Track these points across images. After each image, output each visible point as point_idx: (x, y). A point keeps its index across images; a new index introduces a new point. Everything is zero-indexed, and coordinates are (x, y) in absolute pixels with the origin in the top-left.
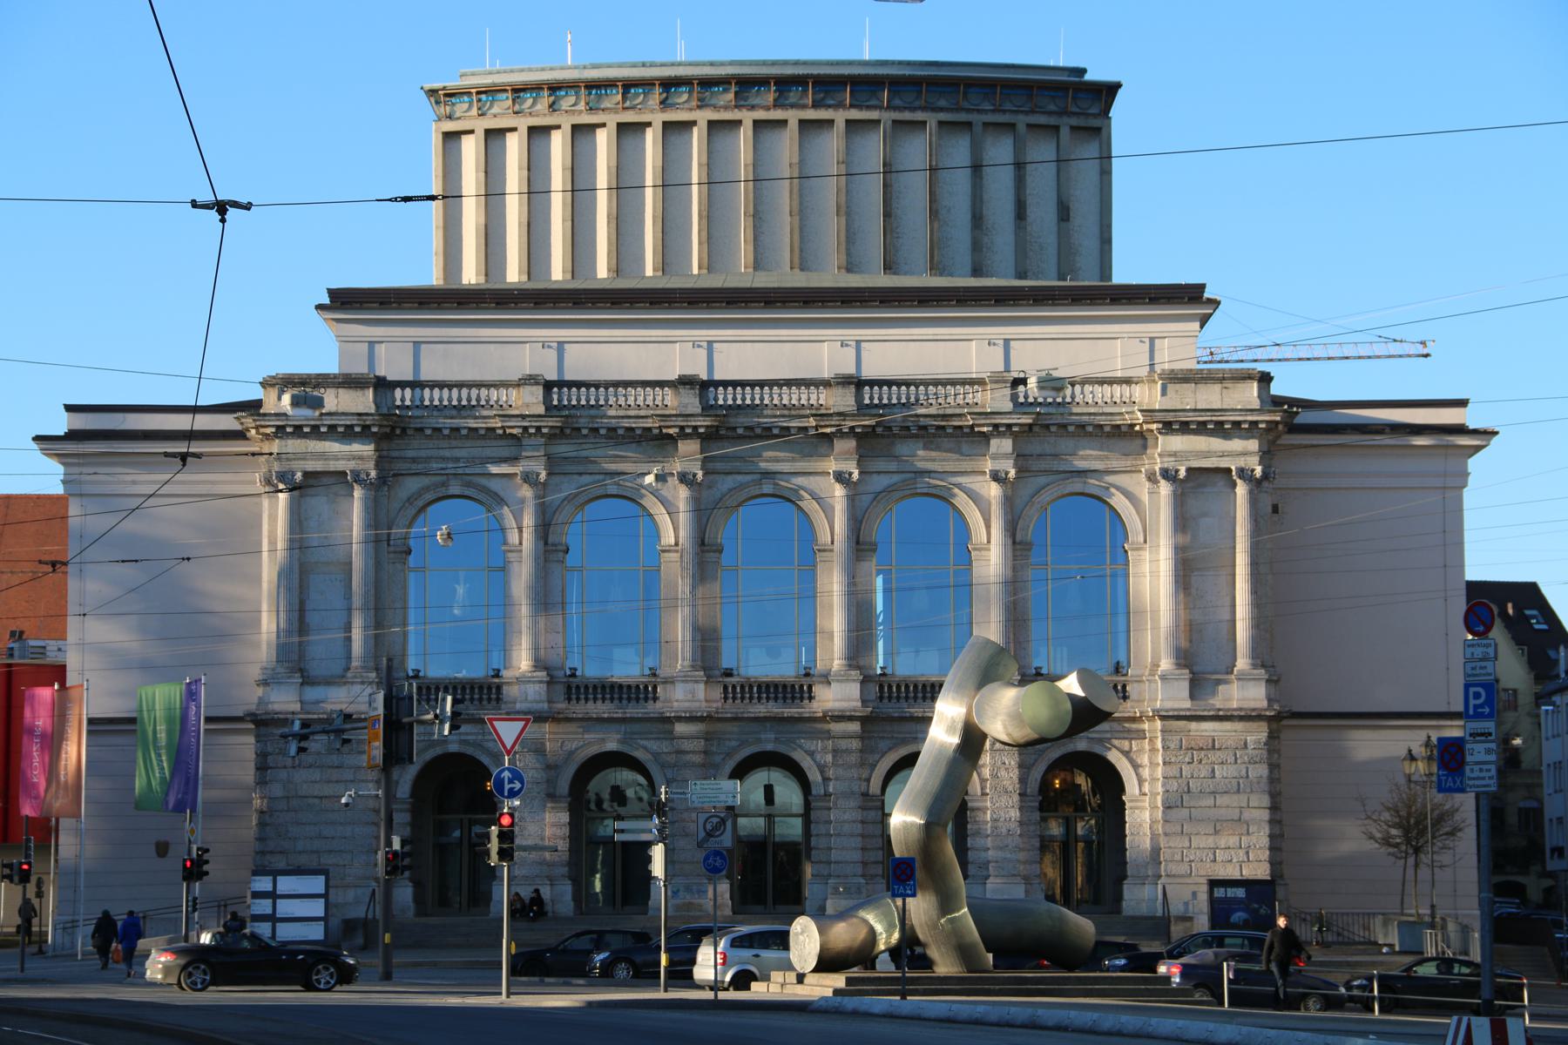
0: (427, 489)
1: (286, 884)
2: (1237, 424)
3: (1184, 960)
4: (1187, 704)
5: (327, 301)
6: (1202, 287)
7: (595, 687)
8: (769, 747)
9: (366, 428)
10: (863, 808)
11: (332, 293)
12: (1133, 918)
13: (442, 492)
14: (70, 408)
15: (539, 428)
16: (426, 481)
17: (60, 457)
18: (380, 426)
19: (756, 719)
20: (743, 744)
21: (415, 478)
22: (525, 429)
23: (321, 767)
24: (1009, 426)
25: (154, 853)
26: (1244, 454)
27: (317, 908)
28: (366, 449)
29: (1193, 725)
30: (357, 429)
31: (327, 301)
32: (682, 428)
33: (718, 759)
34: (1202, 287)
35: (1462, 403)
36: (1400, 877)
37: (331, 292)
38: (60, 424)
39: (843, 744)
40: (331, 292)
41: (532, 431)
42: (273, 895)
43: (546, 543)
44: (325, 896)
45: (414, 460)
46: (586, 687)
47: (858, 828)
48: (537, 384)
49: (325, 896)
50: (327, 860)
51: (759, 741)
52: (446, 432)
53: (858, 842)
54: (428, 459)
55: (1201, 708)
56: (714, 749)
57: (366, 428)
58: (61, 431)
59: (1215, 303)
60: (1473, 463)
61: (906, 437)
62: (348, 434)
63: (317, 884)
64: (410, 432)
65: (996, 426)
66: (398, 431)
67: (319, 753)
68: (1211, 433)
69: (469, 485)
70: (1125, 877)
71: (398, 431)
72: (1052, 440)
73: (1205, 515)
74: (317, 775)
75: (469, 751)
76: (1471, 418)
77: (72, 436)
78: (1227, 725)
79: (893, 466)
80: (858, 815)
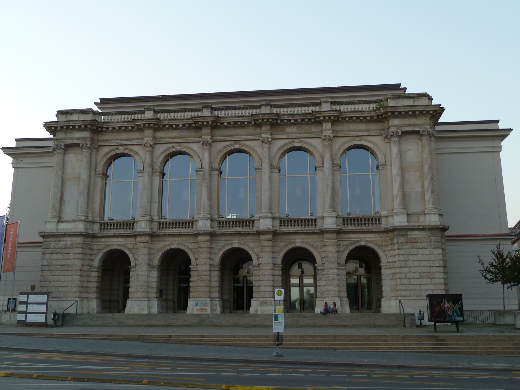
1: (33, 298)
6: (400, 85)
8: (236, 246)
10: (273, 270)
11: (101, 100)
12: (387, 314)
16: (111, 148)
18: (91, 125)
19: (231, 235)
20: (225, 246)
21: (107, 147)
22: (144, 125)
24: (330, 117)
26: (424, 124)
27: (43, 308)
30: (83, 127)
32: (203, 122)
33: (216, 250)
34: (400, 85)
36: (505, 300)
38: (13, 144)
39: (265, 243)
41: (147, 126)
42: (26, 303)
43: (153, 169)
44: (47, 304)
49: (47, 304)
50: (50, 290)
51: (232, 243)
55: (413, 224)
56: (214, 246)
57: (86, 126)
58: (14, 146)
60: (504, 143)
62: (80, 129)
63: (43, 298)
64: (104, 129)
65: (324, 117)
67: (61, 248)
68: (410, 116)
70: (382, 297)
75: (121, 248)
76: (501, 126)
78: (423, 233)
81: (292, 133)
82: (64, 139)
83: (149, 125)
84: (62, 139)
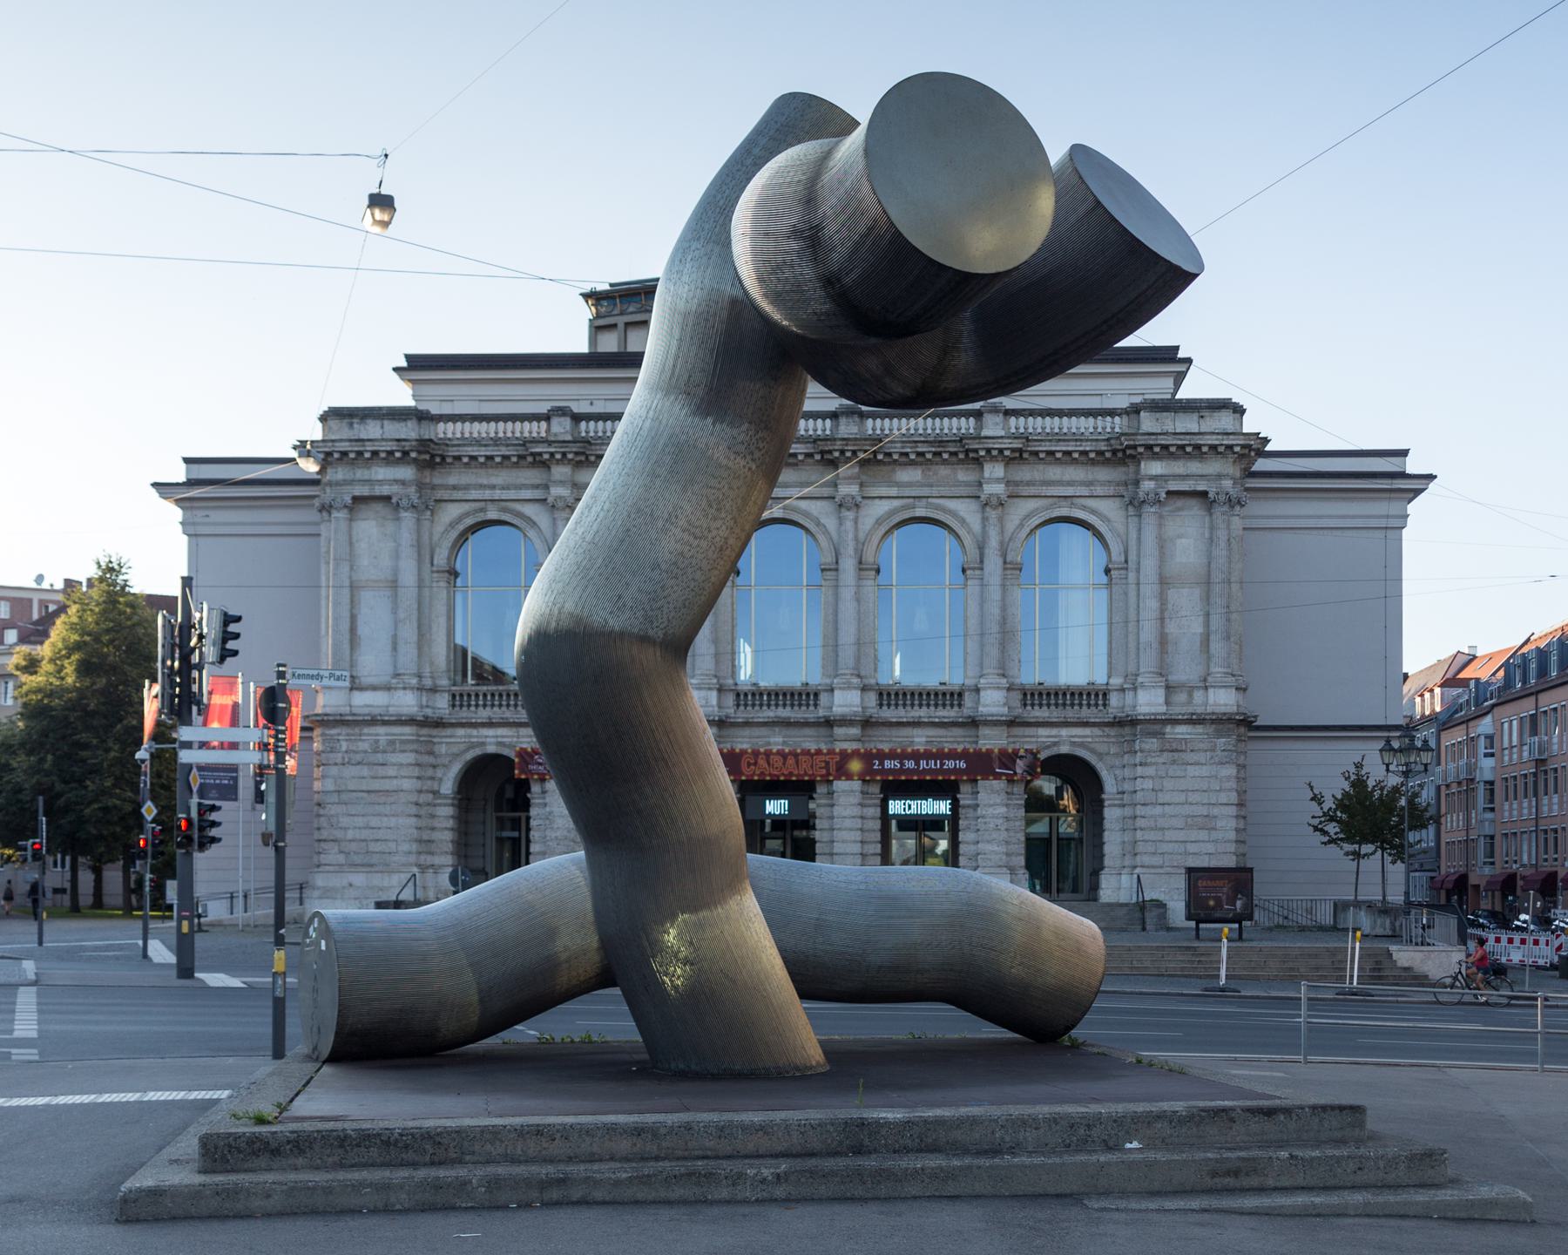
0: (467, 514)
2: (1213, 448)
3: (859, 135)
4: (1163, 709)
5: (404, 364)
6: (1177, 348)
7: (913, 694)
9: (406, 453)
10: (862, 805)
13: (480, 517)
14: (187, 461)
15: (564, 454)
16: (466, 507)
17: (178, 502)
18: (419, 452)
22: (552, 454)
23: (368, 764)
24: (1001, 451)
25: (260, 842)
28: (407, 472)
29: (1168, 729)
31: (404, 364)
34: (1177, 348)
35: (1403, 453)
37: (408, 357)
38: (179, 474)
40: (408, 357)
41: (558, 456)
45: (455, 488)
46: (905, 694)
47: (858, 823)
48: (564, 415)
52: (482, 460)
53: (857, 836)
54: (466, 488)
57: (406, 453)
58: (182, 479)
59: (1189, 361)
60: (1412, 508)
61: (906, 464)
62: (390, 459)
64: (449, 460)
66: (438, 460)
69: (505, 510)
71: (438, 460)
72: (1041, 467)
73: (1180, 536)
74: (365, 771)
75: (469, 756)
76: (1412, 466)
77: (191, 483)
79: (894, 491)
80: (857, 811)
81: (910, 485)
82: (351, 482)
83: (564, 454)
84: (346, 483)
